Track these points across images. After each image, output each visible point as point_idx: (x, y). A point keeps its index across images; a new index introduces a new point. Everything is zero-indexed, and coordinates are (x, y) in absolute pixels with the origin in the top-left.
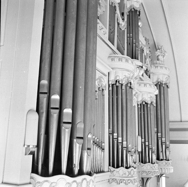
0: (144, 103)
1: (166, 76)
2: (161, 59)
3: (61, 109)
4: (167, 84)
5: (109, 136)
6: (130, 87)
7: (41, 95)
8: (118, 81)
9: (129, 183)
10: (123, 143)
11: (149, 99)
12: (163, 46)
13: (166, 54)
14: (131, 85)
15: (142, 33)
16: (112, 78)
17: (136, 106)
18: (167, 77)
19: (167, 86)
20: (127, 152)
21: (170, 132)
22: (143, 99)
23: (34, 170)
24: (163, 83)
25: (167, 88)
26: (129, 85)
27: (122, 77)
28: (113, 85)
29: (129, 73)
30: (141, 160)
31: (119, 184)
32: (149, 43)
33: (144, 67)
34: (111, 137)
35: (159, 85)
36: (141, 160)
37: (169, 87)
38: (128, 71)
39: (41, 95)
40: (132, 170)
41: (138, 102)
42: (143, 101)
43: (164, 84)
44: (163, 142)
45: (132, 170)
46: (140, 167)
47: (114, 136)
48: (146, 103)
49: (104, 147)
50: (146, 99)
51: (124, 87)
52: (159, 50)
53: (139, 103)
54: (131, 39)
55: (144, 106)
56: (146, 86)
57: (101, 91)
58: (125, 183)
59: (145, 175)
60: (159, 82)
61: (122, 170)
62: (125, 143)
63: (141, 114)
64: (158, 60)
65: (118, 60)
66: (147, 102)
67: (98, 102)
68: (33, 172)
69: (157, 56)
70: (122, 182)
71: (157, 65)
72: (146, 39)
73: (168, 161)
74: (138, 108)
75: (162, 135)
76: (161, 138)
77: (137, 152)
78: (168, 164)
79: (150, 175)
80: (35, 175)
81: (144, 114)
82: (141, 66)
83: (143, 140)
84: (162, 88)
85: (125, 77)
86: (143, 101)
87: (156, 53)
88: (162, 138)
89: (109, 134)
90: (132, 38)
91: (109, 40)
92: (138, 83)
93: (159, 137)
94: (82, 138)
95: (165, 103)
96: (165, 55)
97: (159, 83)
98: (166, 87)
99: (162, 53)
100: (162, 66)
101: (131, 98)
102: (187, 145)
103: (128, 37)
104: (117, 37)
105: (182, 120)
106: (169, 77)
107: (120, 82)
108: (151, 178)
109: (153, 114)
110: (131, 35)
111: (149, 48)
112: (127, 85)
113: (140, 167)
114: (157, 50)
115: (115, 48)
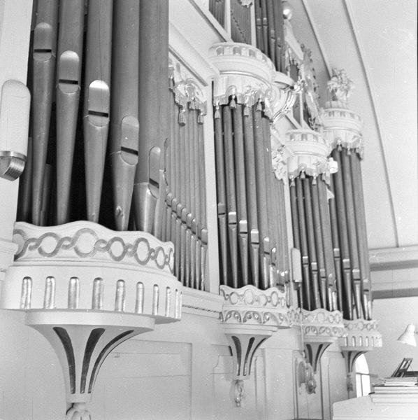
0: (303, 176)
1: (353, 134)
2: (341, 98)
3: (83, 83)
4: (357, 151)
5: (218, 219)
6: (263, 115)
7: (37, 57)
8: (234, 97)
9: (268, 319)
10: (252, 232)
11: (314, 168)
12: (343, 70)
13: (352, 87)
14: (263, 108)
15: (295, 34)
16: (221, 92)
17: (286, 183)
18: (356, 134)
19: (358, 155)
20: (262, 255)
21: (371, 273)
22: (300, 166)
23: (24, 215)
24: (349, 147)
25: (358, 160)
26: (260, 107)
27: (244, 89)
28: (223, 107)
29: (260, 82)
30: (302, 302)
31: (245, 321)
32: (311, 60)
33: (295, 87)
34: (223, 219)
35: (339, 153)
36: (302, 302)
37: (361, 157)
38: (258, 77)
39: (37, 57)
40: (274, 294)
41: (289, 174)
42: (301, 172)
43: (351, 150)
44: (355, 277)
45: (274, 292)
46: (301, 318)
47: (229, 218)
48: (307, 176)
49: (207, 236)
50: (308, 167)
51: (247, 112)
52: (335, 79)
53: (292, 177)
54: (266, 28)
55: (303, 183)
56: (307, 139)
57: (195, 115)
58: (258, 319)
59: (313, 338)
60: (338, 146)
61: (250, 291)
62: (254, 232)
63: (297, 201)
64: (335, 99)
65: (232, 53)
66: (310, 175)
67: (186, 135)
68: (19, 219)
69: (333, 91)
70: (250, 318)
71: (332, 109)
72: (303, 47)
73: (369, 322)
74: (291, 188)
75: (351, 263)
76: (349, 271)
77: (292, 284)
78: (369, 327)
79: (325, 334)
80: (24, 225)
81: (304, 201)
82: (291, 85)
83: (306, 257)
84: (346, 160)
85: (248, 89)
86: (301, 172)
87: (330, 83)
88: (351, 268)
89: (218, 214)
90: (268, 25)
91: (212, 10)
92: (287, 134)
93: (345, 266)
94: (136, 153)
95: (356, 193)
96: (349, 88)
97: (340, 149)
98: (354, 157)
99: (342, 83)
100: (344, 110)
101: (265, 137)
102: (416, 298)
103: (258, 24)
104: (232, 14)
105: (400, 243)
106: (361, 135)
107: (239, 102)
108: (329, 344)
109: (330, 205)
110: (265, 19)
111: (313, 69)
112: (254, 107)
113: (301, 318)
114: (330, 78)
115: (227, 34)
